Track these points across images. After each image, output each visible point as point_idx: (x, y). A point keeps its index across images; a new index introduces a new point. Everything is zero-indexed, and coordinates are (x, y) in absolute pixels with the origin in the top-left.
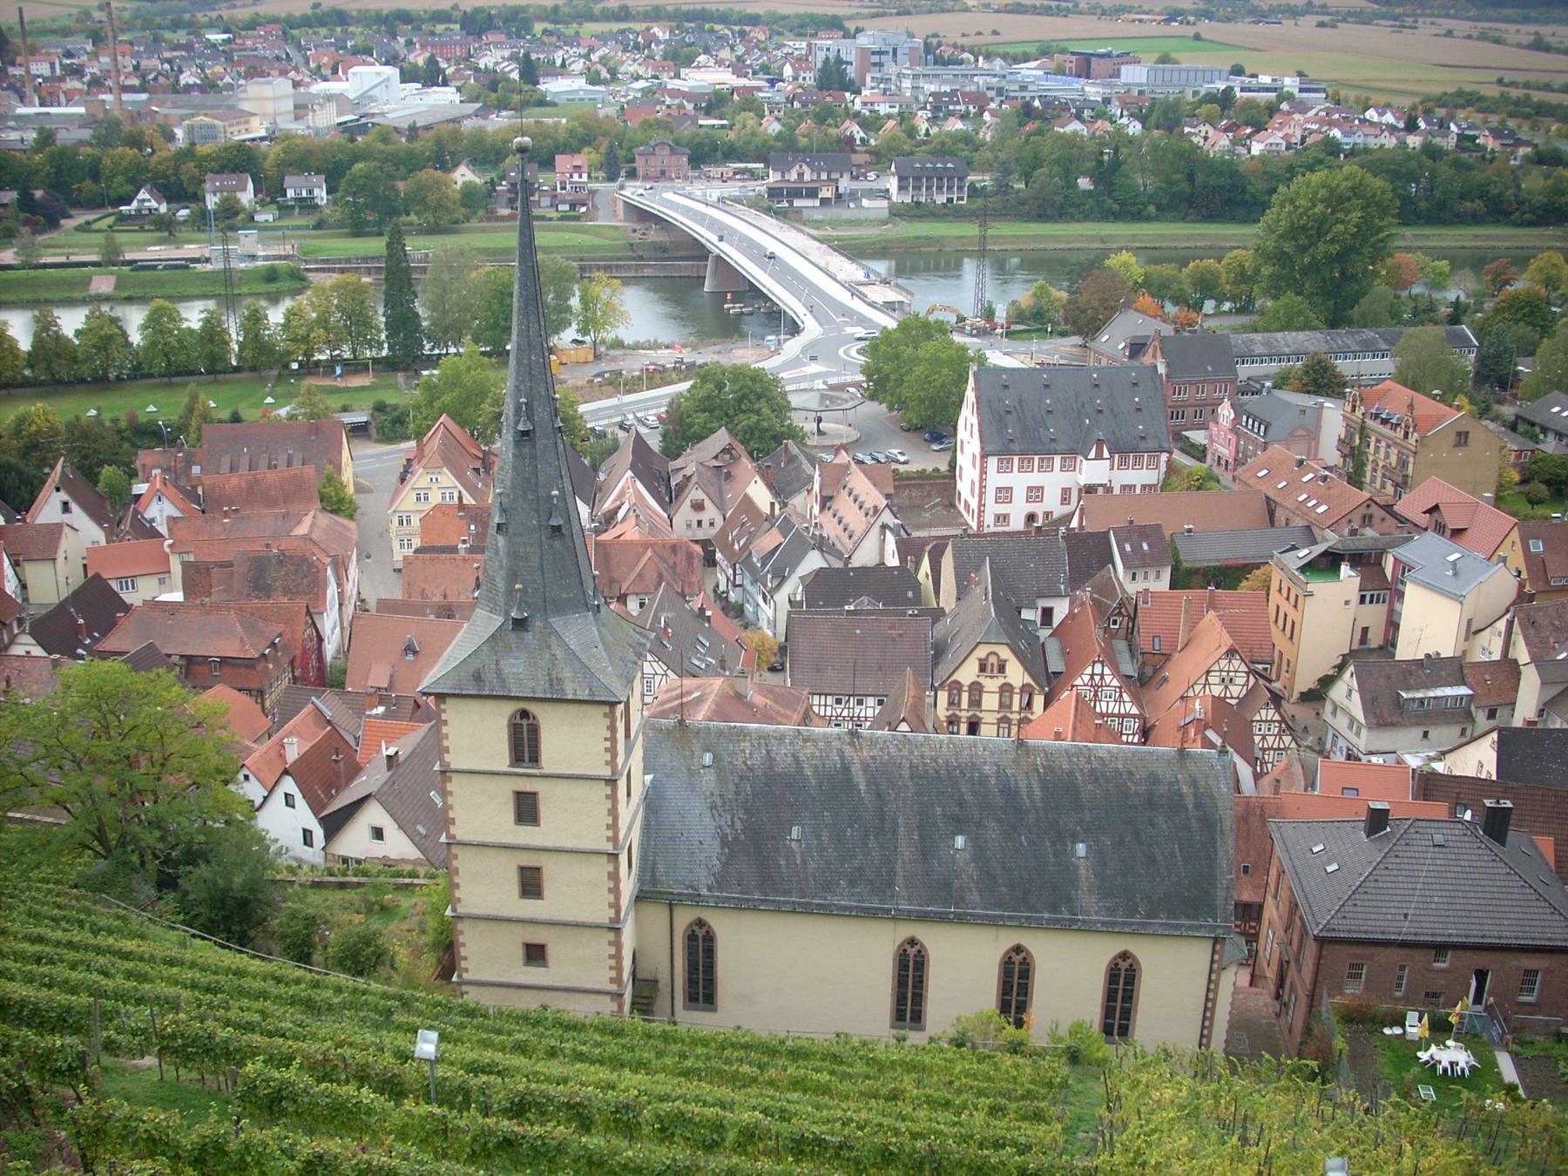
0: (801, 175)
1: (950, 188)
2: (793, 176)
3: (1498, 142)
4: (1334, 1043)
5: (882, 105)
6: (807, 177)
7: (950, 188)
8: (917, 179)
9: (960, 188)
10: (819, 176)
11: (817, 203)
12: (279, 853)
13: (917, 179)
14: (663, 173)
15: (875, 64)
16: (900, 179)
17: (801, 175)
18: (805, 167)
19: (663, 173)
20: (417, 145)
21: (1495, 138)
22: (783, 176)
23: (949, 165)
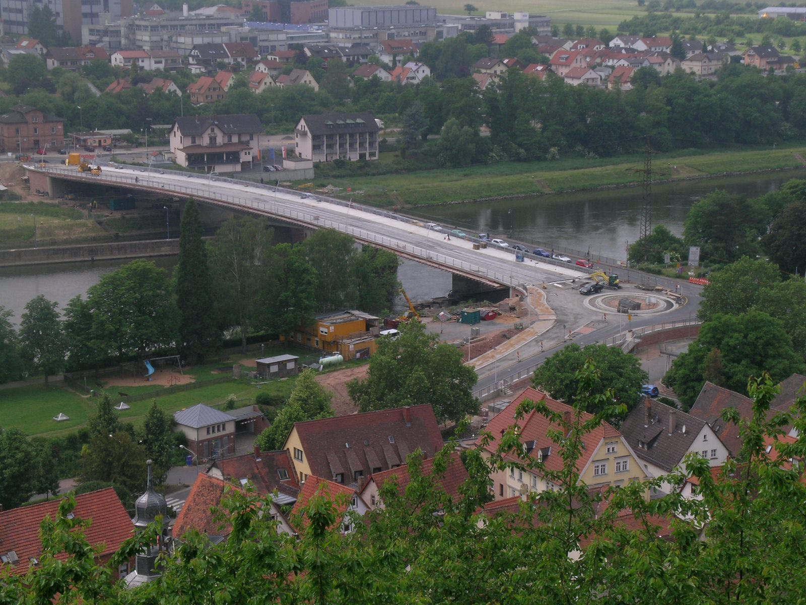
0: (213, 139)
1: (361, 145)
2: (206, 141)
3: (764, 61)
4: (622, 447)
5: (147, 62)
6: (220, 140)
7: (330, 146)
8: (330, 137)
9: (371, 144)
10: (230, 140)
11: (238, 168)
12: (101, 281)
13: (330, 137)
14: (37, 143)
15: (85, 15)
16: (315, 138)
17: (213, 139)
18: (217, 131)
19: (37, 143)
20: (698, 483)
21: (761, 57)
22: (194, 142)
23: (359, 121)
